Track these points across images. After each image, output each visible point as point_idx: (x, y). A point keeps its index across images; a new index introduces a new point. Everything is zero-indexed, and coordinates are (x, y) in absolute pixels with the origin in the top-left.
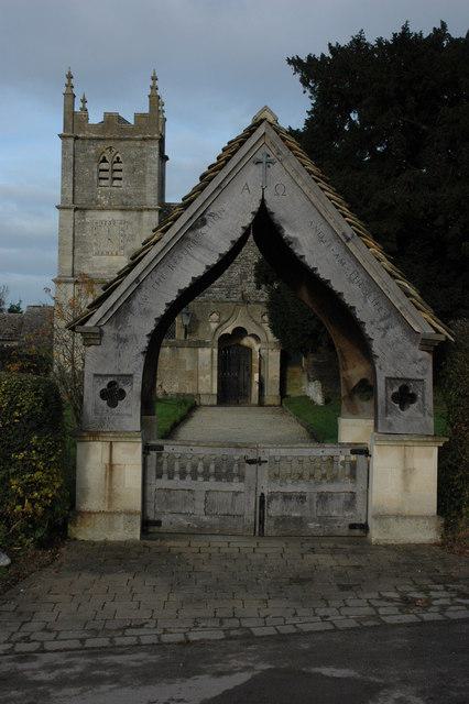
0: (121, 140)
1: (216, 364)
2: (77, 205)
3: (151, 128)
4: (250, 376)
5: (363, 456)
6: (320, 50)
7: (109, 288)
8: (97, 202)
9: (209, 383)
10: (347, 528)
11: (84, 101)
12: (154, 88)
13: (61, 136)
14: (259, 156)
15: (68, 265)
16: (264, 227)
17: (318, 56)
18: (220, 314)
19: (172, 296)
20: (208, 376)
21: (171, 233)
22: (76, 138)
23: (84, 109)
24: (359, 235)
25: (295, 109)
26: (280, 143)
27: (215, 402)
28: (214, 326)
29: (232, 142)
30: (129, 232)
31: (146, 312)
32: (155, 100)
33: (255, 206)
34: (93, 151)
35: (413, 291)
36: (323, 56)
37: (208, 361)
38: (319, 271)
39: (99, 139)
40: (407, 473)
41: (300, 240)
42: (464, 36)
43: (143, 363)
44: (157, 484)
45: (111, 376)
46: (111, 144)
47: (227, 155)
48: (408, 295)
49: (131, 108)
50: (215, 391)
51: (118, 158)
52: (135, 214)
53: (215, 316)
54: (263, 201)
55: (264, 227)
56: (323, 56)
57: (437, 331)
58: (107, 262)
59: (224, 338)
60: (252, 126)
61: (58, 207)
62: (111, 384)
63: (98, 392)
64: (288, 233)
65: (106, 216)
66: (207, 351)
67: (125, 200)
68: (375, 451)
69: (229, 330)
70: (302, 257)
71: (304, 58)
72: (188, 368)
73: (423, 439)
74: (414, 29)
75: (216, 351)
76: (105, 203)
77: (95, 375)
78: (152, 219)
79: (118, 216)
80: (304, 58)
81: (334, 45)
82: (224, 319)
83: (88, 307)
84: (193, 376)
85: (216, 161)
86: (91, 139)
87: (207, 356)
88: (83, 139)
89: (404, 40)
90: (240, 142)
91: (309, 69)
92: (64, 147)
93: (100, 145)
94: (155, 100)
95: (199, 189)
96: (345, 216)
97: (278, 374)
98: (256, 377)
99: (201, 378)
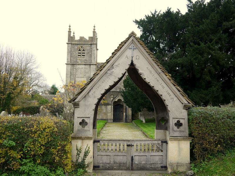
0: (84, 44)
1: (112, 110)
2: (72, 64)
3: (93, 41)
4: (123, 114)
5: (165, 143)
6: (143, 17)
7: (83, 90)
8: (78, 62)
9: (110, 115)
10: (160, 168)
11: (74, 33)
12: (94, 29)
13: (67, 43)
14: (130, 47)
15: (69, 81)
16: (132, 70)
17: (143, 19)
18: (114, 96)
19: (103, 92)
20: (110, 114)
21: (103, 71)
22: (72, 44)
23: (74, 36)
24: (163, 72)
25: (139, 33)
26: (137, 43)
27: (112, 121)
28: (112, 99)
29: (122, 42)
30: (87, 71)
31: (95, 97)
32: (94, 32)
33: (130, 63)
34: (76, 48)
35: (181, 90)
36: (144, 19)
37: (110, 109)
38: (150, 83)
39: (78, 44)
40: (180, 150)
41: (144, 74)
42: (184, 11)
43: (94, 113)
44: (97, 153)
45: (83, 117)
46: (82, 45)
47: (121, 46)
48: (179, 91)
49: (88, 35)
50: (112, 118)
51: (84, 50)
52: (88, 66)
53: (112, 96)
54: (132, 61)
55: (132, 70)
56: (144, 19)
57: (189, 103)
58: (82, 80)
59: (115, 102)
60: (128, 38)
61: (66, 64)
62: (83, 120)
63: (79, 123)
64: (140, 71)
65: (81, 66)
66: (110, 106)
67: (85, 61)
68: (169, 142)
69: (116, 100)
70: (145, 79)
71: (139, 20)
72: (104, 111)
73: (184, 138)
74: (171, 10)
75: (112, 106)
76: (80, 63)
77: (78, 117)
78: (93, 68)
79: (83, 66)
80: (139, 20)
81: (147, 15)
82: (115, 97)
83: (76, 95)
84: (106, 114)
85: (117, 48)
86: (76, 44)
87: (110, 108)
88: (73, 44)
89: (169, 13)
90: (125, 42)
91: (140, 23)
92: (68, 46)
93: (79, 46)
94: (94, 32)
95: (112, 57)
96: (158, 66)
97: (131, 113)
98: (125, 114)
99: (108, 114)
